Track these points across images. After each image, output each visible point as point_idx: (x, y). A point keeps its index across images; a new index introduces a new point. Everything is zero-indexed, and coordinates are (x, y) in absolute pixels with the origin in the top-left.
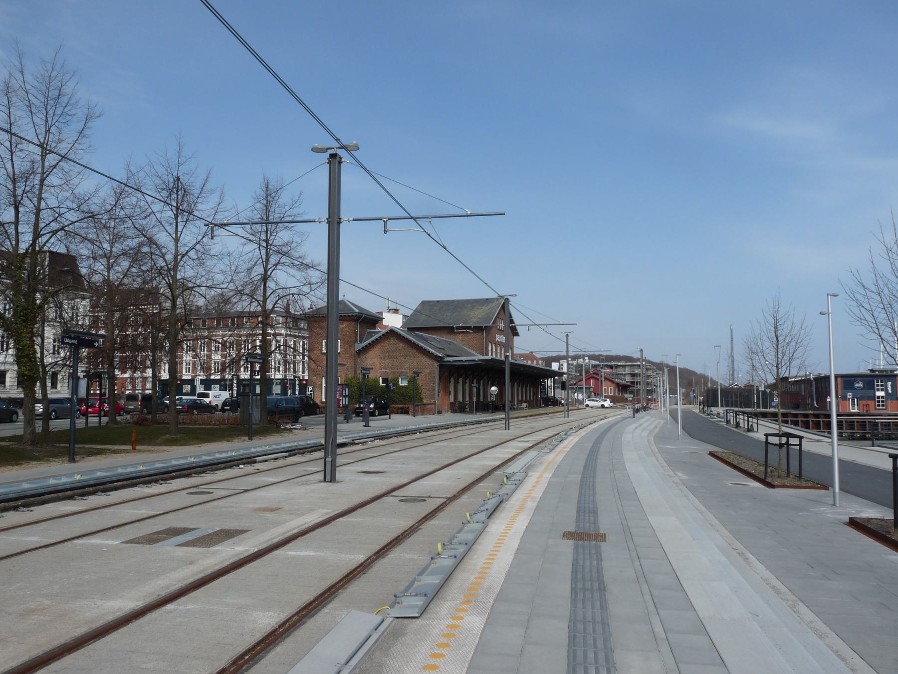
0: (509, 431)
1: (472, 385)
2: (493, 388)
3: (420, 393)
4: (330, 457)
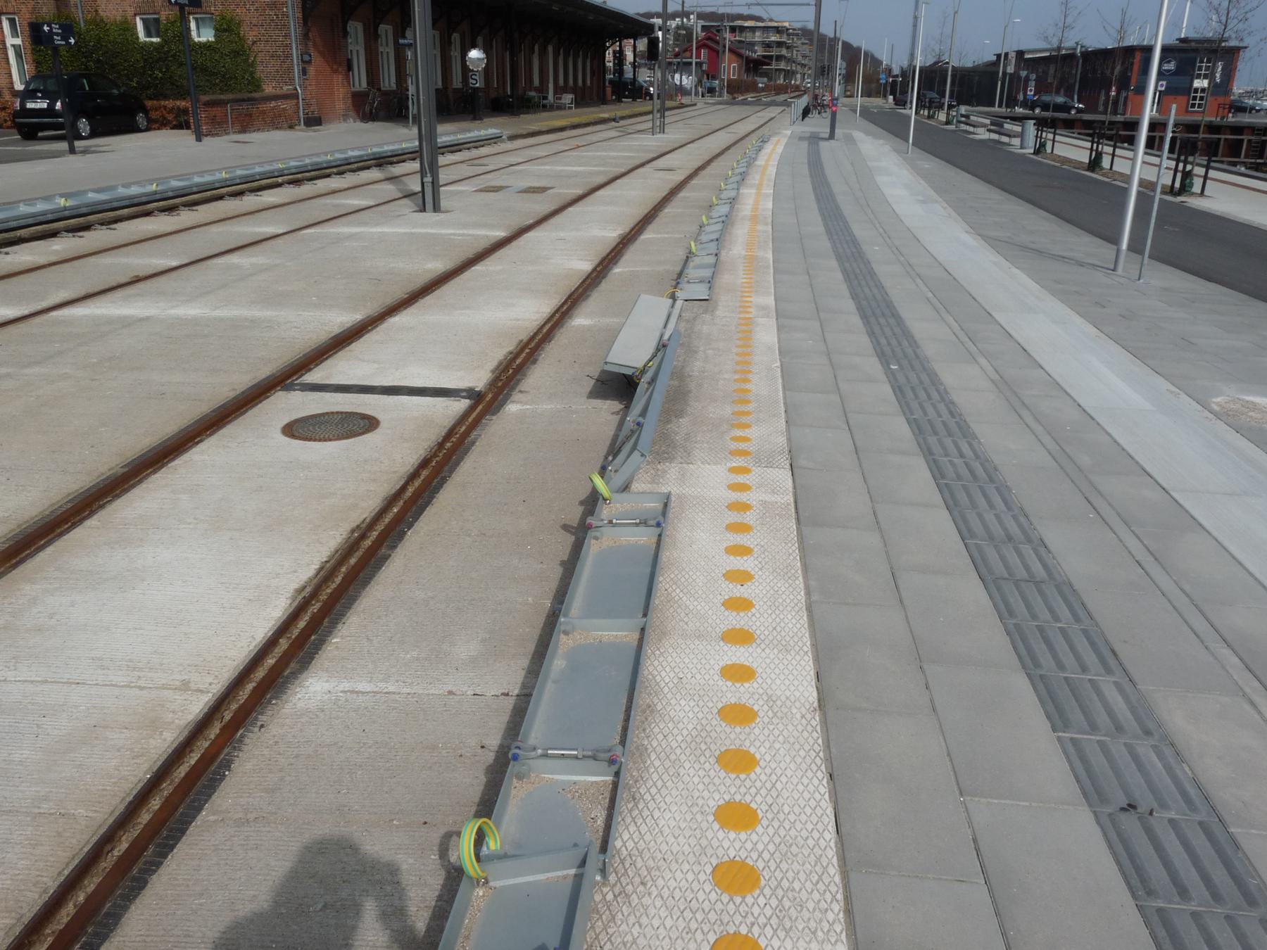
0: (665, 136)
1: (401, 41)
2: (474, 54)
3: (252, 65)
4: (429, 175)
